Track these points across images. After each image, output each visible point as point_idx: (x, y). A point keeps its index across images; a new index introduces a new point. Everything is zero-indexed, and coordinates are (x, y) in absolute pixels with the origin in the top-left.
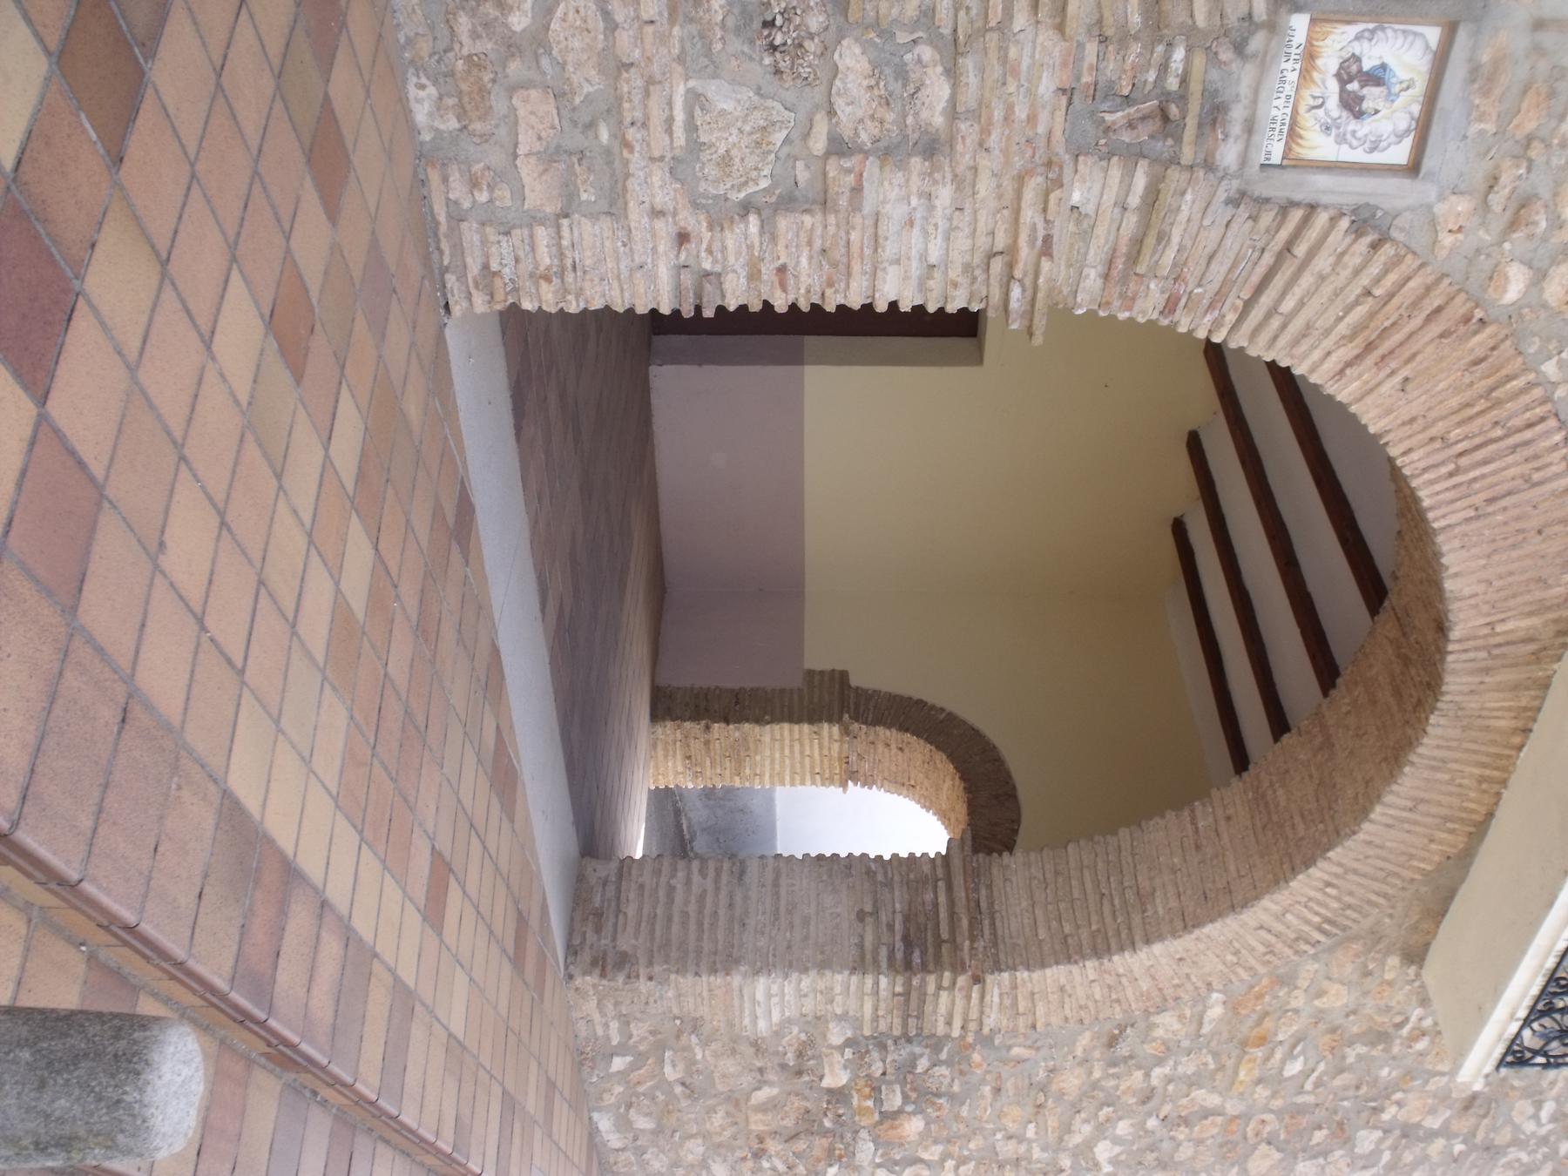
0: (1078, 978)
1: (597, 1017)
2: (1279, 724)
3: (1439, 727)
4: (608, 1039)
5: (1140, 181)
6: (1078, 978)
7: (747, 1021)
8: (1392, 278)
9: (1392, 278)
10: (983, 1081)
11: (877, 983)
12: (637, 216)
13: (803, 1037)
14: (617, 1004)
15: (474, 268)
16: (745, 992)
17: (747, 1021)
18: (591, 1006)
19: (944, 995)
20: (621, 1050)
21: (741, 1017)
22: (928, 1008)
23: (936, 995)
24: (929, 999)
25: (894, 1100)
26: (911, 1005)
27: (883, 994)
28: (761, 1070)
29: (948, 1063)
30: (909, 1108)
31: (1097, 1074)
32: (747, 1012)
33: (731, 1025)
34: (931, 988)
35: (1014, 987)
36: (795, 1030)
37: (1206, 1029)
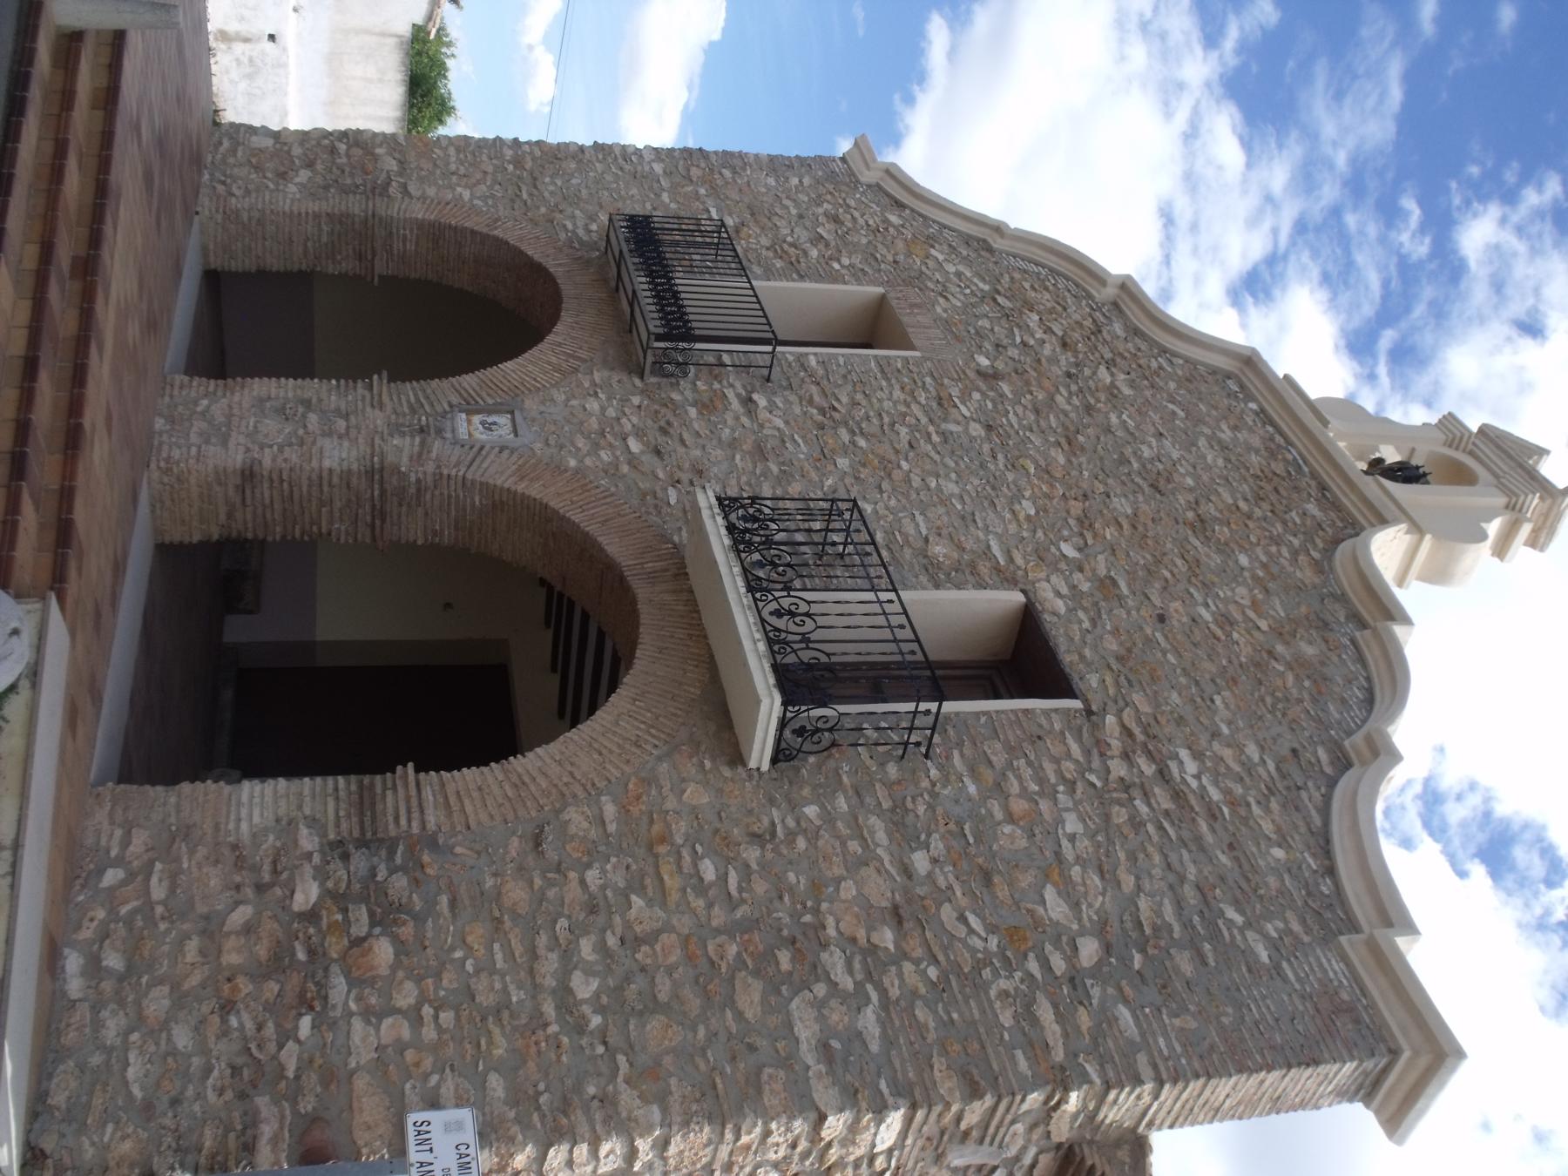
0: (490, 780)
1: (106, 825)
2: (991, 1144)
3: (642, 607)
4: (108, 852)
5: (417, 440)
6: (490, 780)
7: (231, 826)
8: (1178, 1105)
9: (1178, 1105)
10: (439, 892)
11: (336, 783)
12: (232, 444)
13: (278, 844)
14: (125, 809)
15: (164, 455)
16: (233, 798)
17: (231, 826)
18: (101, 816)
19: (389, 793)
20: (119, 862)
21: (227, 824)
22: (379, 807)
23: (384, 796)
24: (378, 798)
25: (361, 926)
26: (365, 805)
27: (342, 794)
28: (238, 888)
29: (403, 869)
30: (377, 930)
31: (538, 882)
32: (233, 817)
33: (217, 828)
34: (379, 790)
35: (443, 785)
36: (271, 838)
37: (612, 828)
